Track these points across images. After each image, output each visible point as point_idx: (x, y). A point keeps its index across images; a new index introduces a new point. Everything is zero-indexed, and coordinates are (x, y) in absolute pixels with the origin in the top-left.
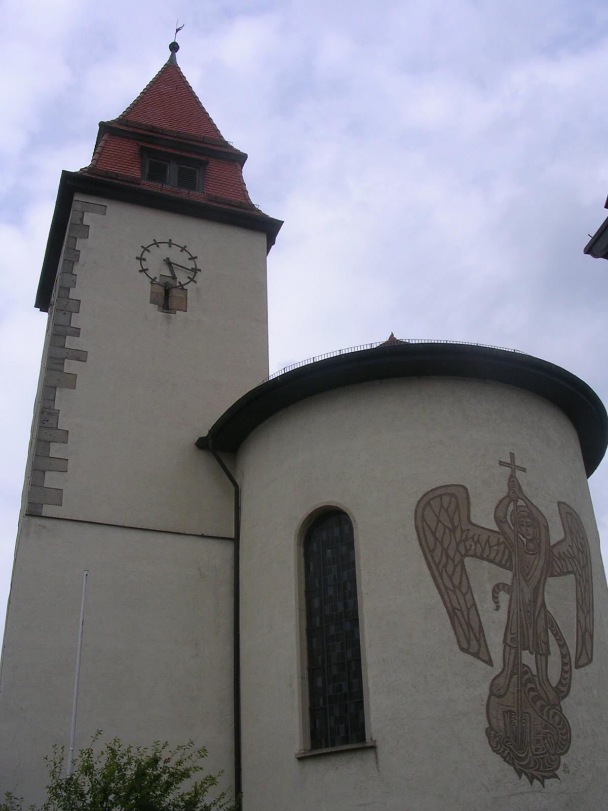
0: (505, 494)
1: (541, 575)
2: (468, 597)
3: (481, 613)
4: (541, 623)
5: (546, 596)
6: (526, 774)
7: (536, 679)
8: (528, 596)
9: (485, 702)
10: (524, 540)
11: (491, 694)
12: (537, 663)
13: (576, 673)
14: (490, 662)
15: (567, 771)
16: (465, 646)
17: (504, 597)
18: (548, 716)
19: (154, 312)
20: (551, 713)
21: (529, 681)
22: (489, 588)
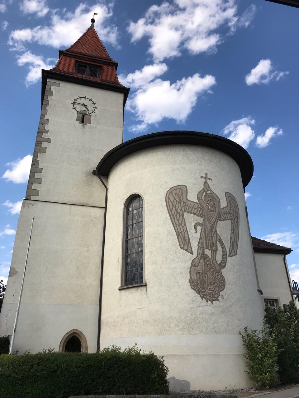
0: (202, 189)
1: (216, 220)
2: (185, 227)
3: (189, 234)
4: (214, 238)
5: (217, 228)
6: (205, 298)
7: (211, 260)
8: (209, 227)
9: (189, 268)
10: (209, 206)
12: (211, 254)
13: (229, 259)
14: (192, 253)
15: (222, 298)
16: (182, 246)
17: (199, 228)
18: (215, 275)
19: (78, 124)
20: (217, 274)
21: (208, 261)
22: (193, 224)
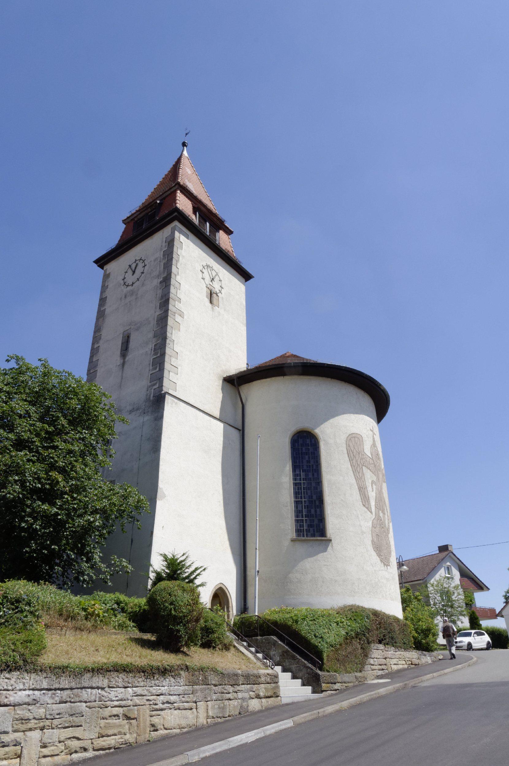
11: (373, 526)
